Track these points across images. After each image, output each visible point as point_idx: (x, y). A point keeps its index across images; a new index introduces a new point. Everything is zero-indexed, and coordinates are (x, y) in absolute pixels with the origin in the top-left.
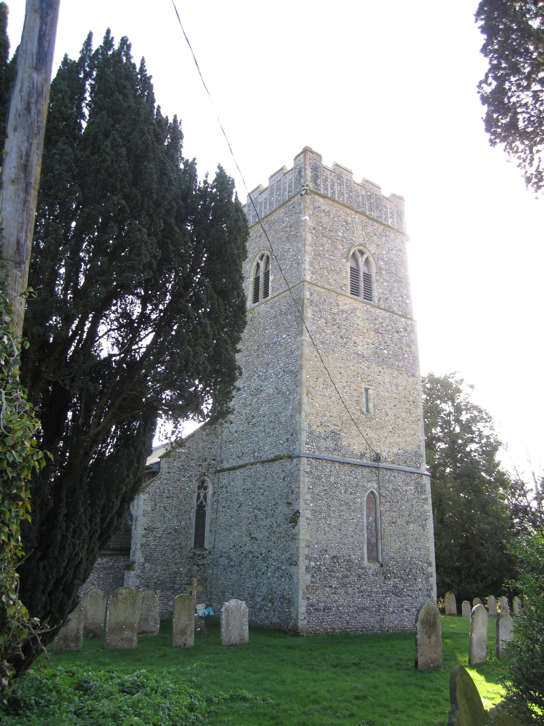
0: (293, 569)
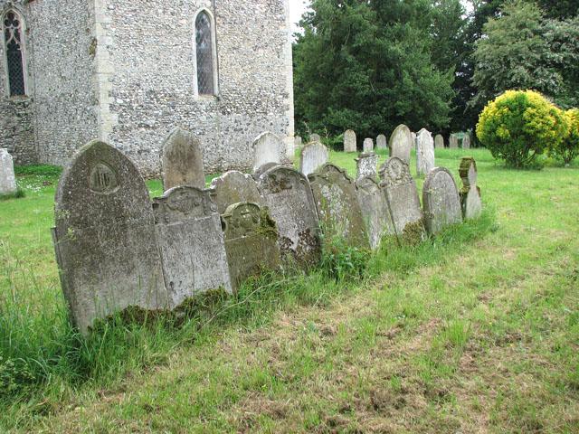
0: (96, 109)
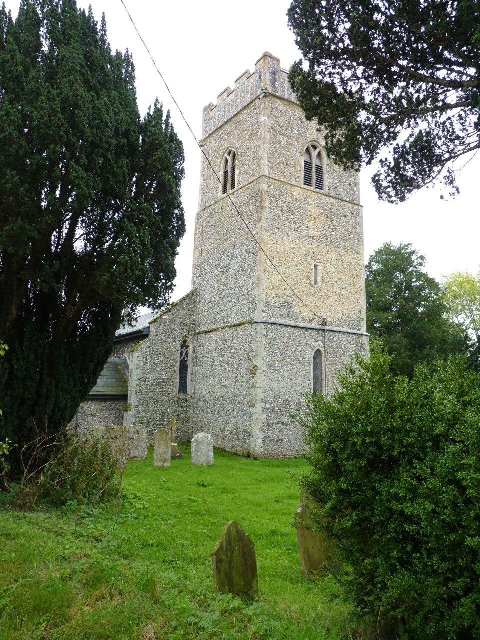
0: (253, 410)
